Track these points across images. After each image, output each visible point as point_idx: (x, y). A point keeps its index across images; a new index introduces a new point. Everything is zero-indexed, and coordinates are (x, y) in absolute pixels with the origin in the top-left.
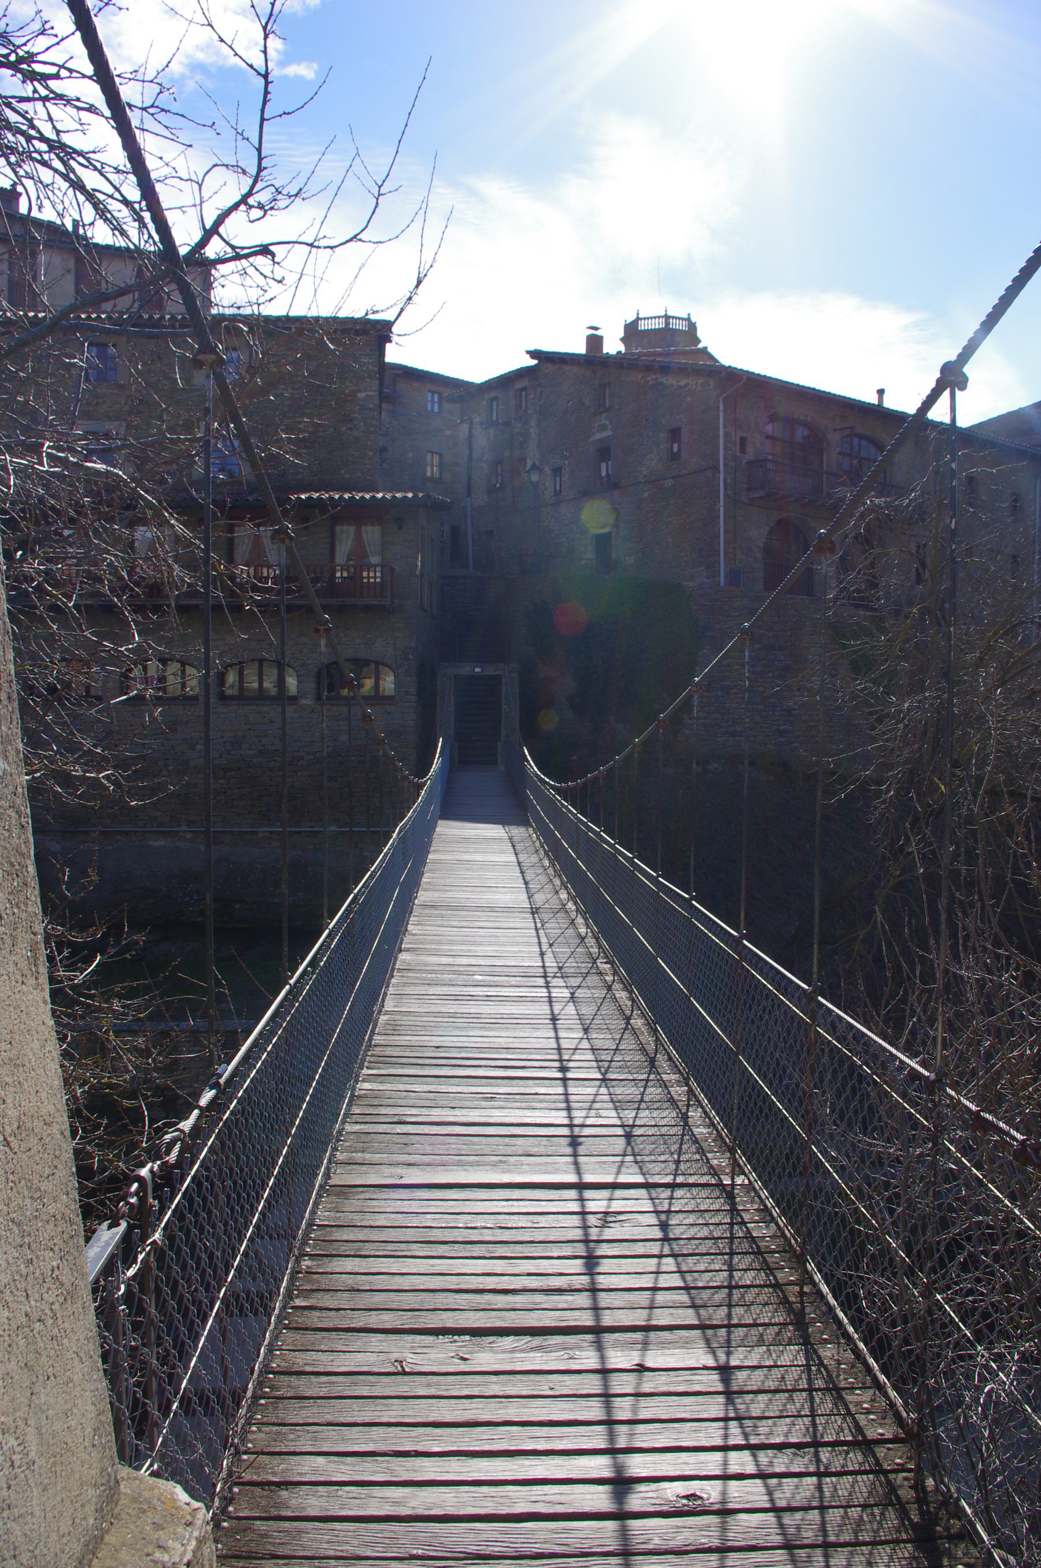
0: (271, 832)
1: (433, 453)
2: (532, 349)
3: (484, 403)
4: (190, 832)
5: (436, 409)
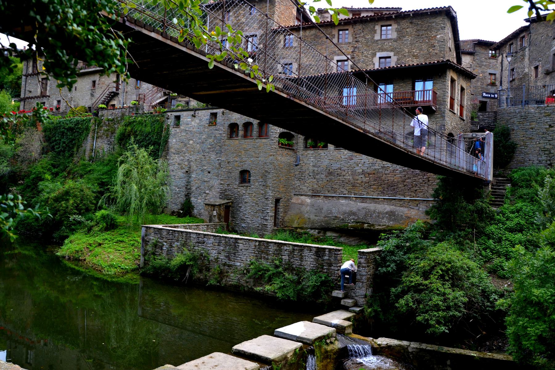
0: (384, 199)
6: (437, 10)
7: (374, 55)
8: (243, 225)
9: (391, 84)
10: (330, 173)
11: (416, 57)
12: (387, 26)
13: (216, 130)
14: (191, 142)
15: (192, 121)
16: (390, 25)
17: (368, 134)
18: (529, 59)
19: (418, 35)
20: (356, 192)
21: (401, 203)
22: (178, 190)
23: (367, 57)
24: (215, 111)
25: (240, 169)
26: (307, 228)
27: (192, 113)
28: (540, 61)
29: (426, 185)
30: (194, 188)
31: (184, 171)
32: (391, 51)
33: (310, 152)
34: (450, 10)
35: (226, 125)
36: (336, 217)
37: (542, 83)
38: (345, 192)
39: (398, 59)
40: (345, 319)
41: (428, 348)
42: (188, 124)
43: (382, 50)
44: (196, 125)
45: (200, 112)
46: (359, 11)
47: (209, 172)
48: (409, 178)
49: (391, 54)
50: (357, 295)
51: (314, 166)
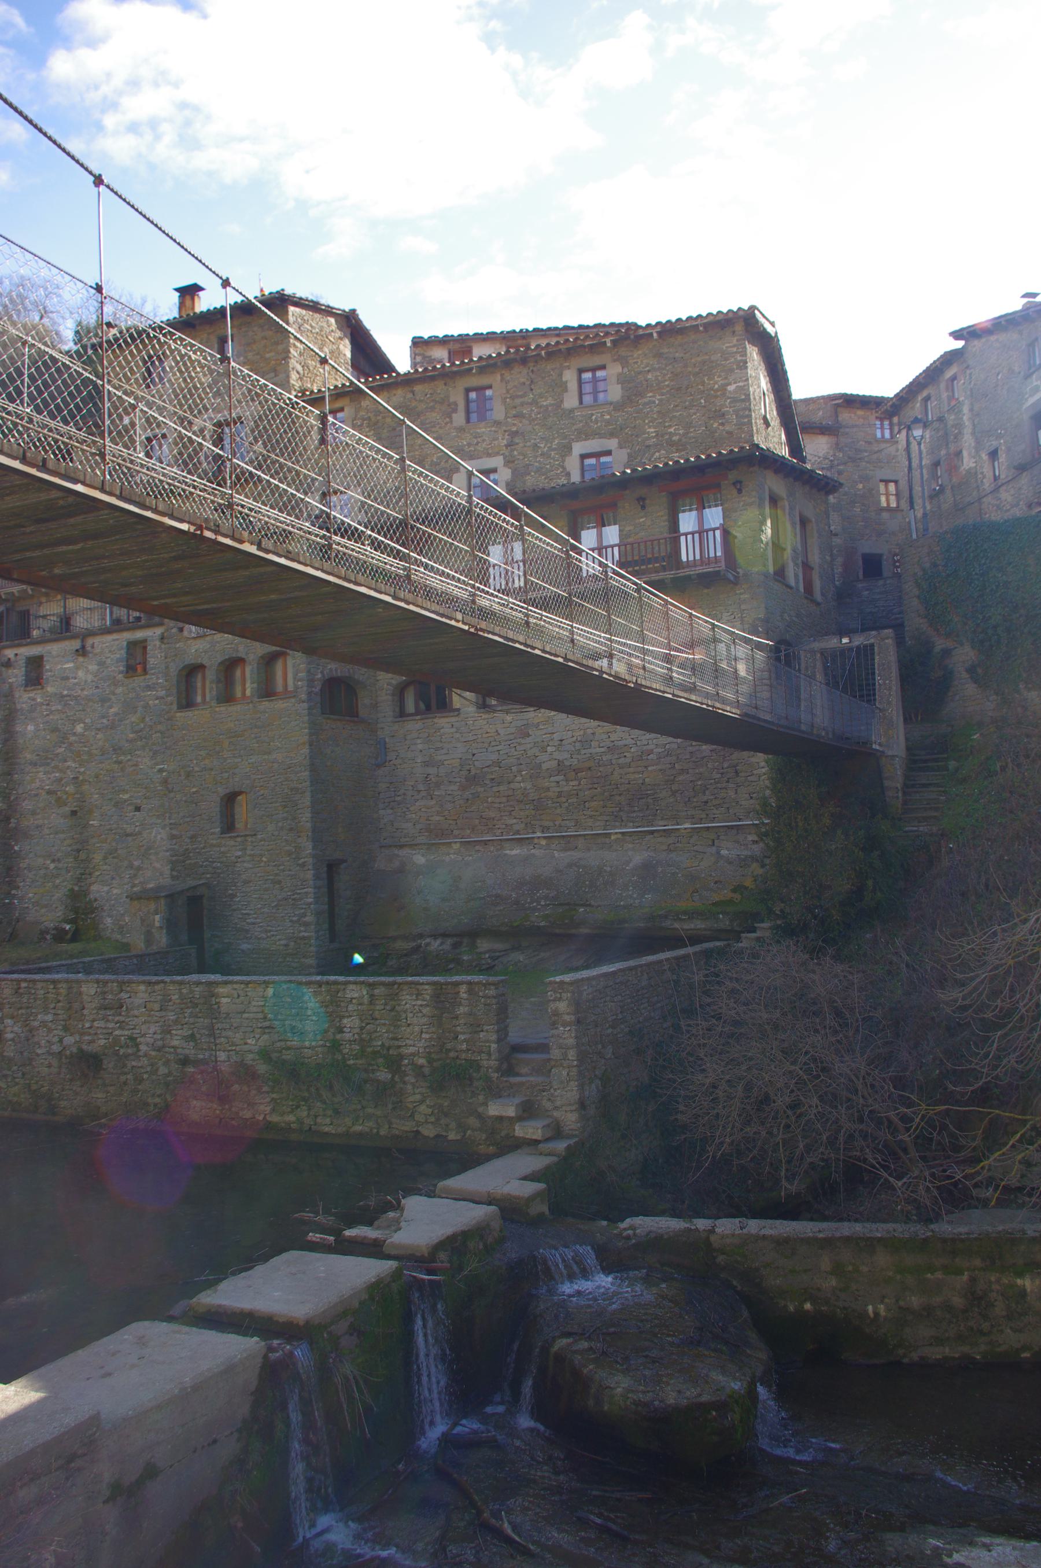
0: (623, 833)
1: (887, 482)
2: (957, 328)
3: (918, 405)
4: (545, 838)
5: (887, 435)
6: (721, 317)
7: (567, 449)
8: (245, 946)
9: (615, 524)
10: (472, 780)
11: (680, 446)
12: (593, 370)
13: (149, 688)
14: (79, 728)
15: (77, 668)
16: (603, 367)
17: (481, 633)
18: (973, 433)
19: (679, 389)
20: (546, 824)
21: (670, 841)
22: (52, 866)
23: (549, 457)
24: (139, 635)
25: (222, 791)
26: (421, 936)
27: (76, 644)
28: (999, 437)
29: (731, 785)
30: (98, 857)
31: (67, 809)
32: (612, 435)
33: (414, 726)
34: (754, 316)
35: (174, 670)
36: (497, 896)
37: (1012, 492)
38: (516, 827)
39: (630, 455)
40: (525, 1178)
41: (767, 1232)
42: (67, 678)
43: (585, 435)
44: (90, 678)
45: (97, 640)
46: (524, 338)
47: (138, 809)
48: (683, 771)
49: (612, 444)
50: (558, 1103)
51: (426, 764)
